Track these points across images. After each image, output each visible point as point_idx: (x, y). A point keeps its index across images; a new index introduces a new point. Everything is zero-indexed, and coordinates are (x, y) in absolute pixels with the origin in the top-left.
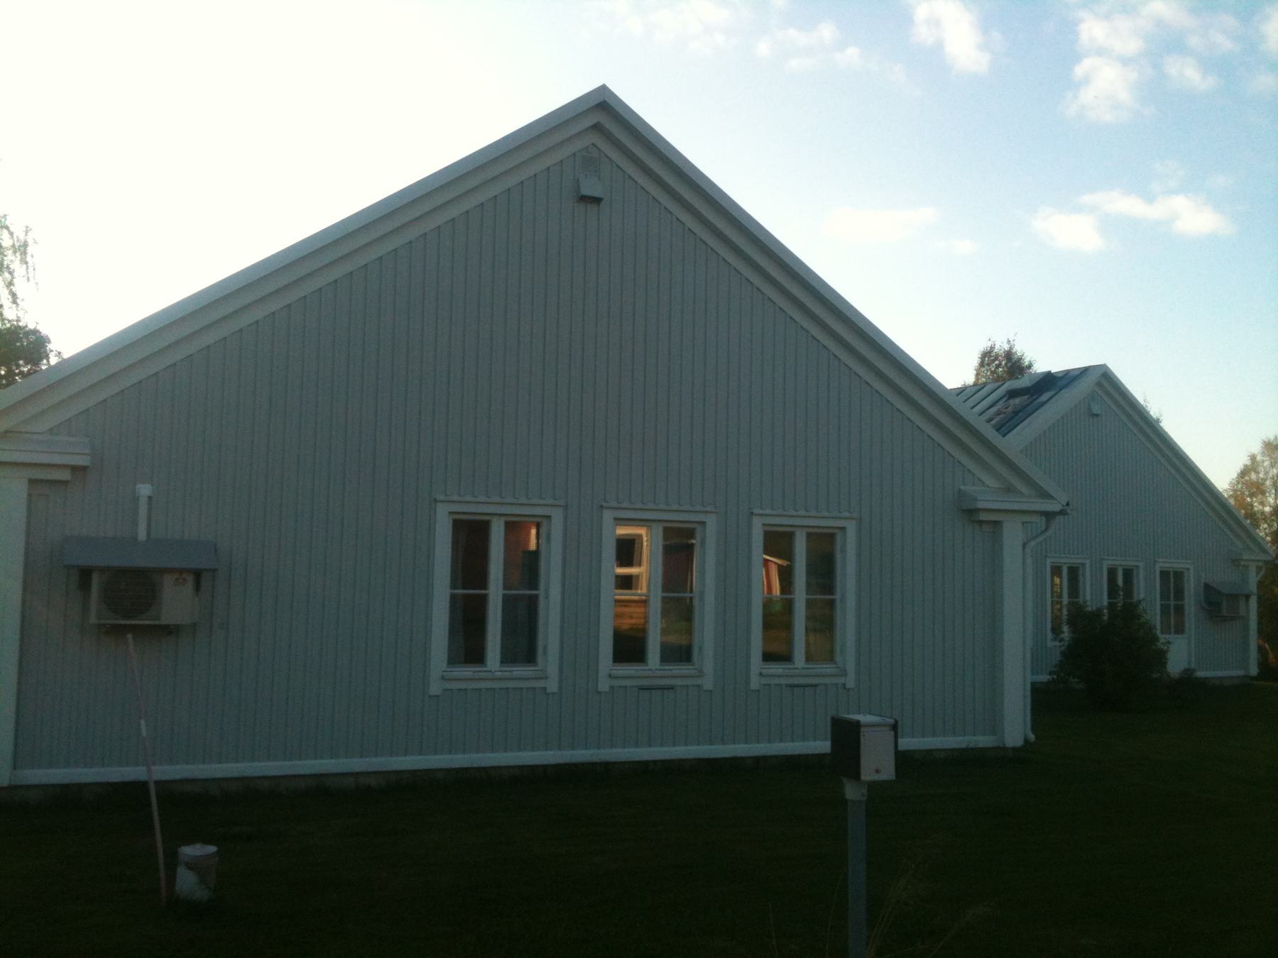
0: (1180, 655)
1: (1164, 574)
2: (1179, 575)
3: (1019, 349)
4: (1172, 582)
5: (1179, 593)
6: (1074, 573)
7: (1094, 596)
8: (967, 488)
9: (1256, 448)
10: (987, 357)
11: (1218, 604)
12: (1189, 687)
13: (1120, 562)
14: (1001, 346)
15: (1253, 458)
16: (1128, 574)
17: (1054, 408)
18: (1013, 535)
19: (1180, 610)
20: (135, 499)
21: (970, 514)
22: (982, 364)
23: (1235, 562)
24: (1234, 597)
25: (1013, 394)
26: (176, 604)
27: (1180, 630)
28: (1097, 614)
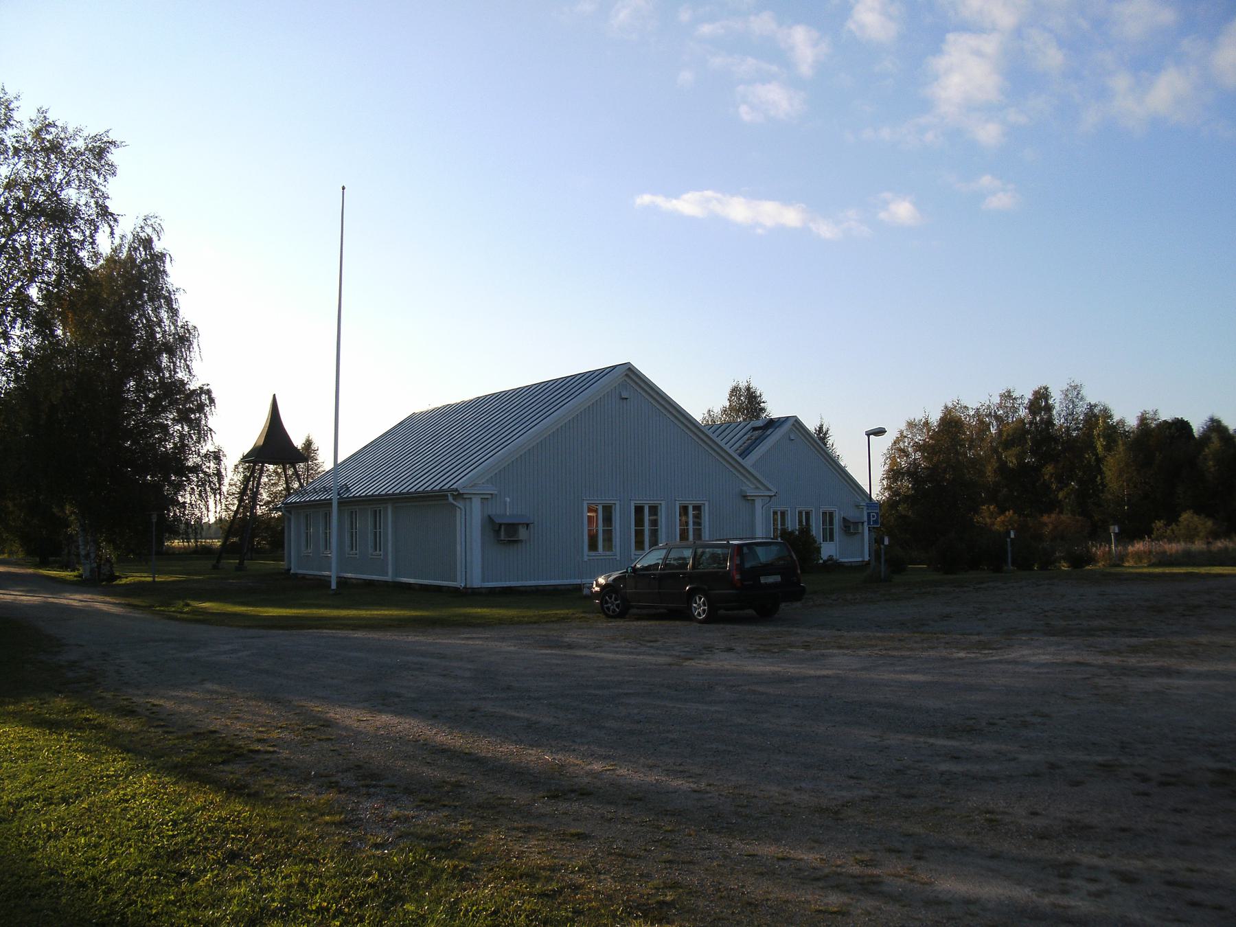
0: (828, 550)
1: (824, 513)
2: (831, 514)
3: (754, 385)
4: (828, 517)
5: (831, 523)
6: (608, 510)
7: (792, 525)
8: (744, 488)
9: (903, 426)
10: (735, 391)
11: (850, 527)
12: (833, 566)
13: (804, 508)
14: (743, 385)
15: (901, 432)
16: (808, 514)
17: (776, 436)
18: (759, 503)
19: (831, 531)
20: (505, 502)
21: (745, 497)
22: (731, 395)
23: (857, 506)
24: (856, 524)
25: (755, 429)
26: (523, 533)
27: (832, 539)
28: (792, 533)
